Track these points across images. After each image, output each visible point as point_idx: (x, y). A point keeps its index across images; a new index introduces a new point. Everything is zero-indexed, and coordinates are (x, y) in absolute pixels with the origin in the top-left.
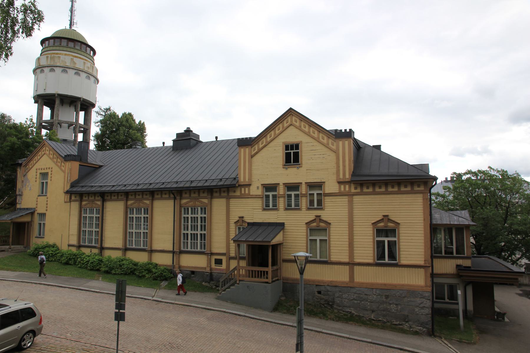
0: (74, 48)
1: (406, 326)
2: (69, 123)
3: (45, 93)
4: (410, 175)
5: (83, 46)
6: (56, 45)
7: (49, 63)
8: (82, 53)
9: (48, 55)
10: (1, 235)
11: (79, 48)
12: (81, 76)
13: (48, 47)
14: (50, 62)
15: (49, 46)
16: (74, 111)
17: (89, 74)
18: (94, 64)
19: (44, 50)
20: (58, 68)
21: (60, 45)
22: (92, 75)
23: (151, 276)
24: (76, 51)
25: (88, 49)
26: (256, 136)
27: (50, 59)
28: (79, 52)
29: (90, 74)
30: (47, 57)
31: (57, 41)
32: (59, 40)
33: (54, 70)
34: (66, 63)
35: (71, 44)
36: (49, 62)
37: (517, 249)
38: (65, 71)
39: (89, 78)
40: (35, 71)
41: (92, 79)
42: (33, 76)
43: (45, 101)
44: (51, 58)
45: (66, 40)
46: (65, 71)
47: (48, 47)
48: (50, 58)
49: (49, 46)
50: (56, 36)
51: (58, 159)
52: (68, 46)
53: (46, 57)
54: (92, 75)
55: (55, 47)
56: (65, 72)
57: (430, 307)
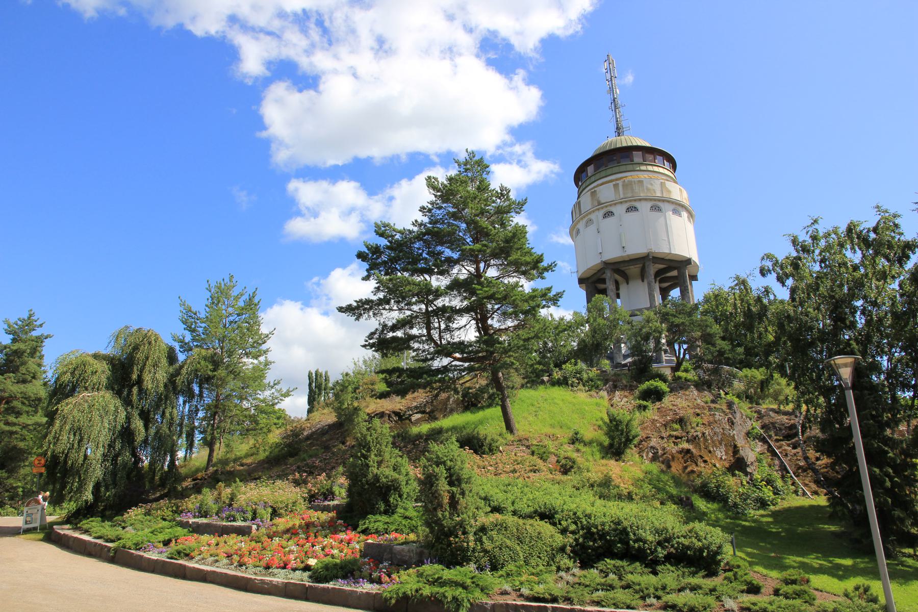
4: (663, 259)
7: (622, 196)
9: (618, 182)
10: (914, 422)
11: (641, 160)
12: (639, 209)
14: (624, 194)
17: (655, 200)
20: (644, 203)
22: (663, 201)
27: (623, 188)
29: (659, 200)
30: (616, 186)
33: (377, 233)
34: (655, 192)
36: (621, 192)
37: (484, 354)
39: (659, 209)
44: (625, 186)
45: (640, 153)
48: (623, 185)
53: (612, 186)
54: (663, 201)
57: (462, 469)
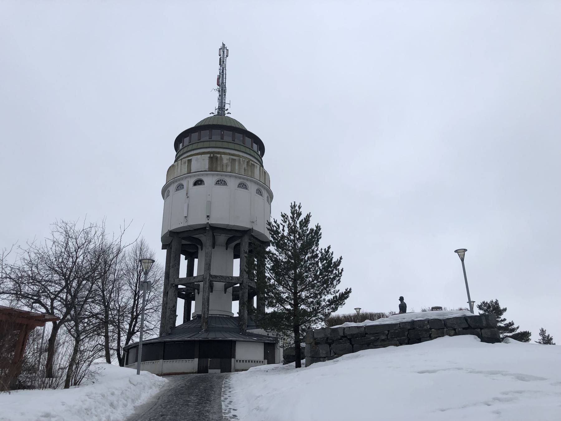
0: (211, 140)
1: (203, 306)
2: (227, 280)
3: (186, 225)
5: (239, 136)
6: (214, 138)
8: (237, 147)
11: (230, 139)
13: (188, 146)
15: (191, 143)
16: (232, 255)
18: (263, 167)
19: (178, 155)
21: (199, 140)
23: (37, 282)
24: (225, 145)
25: (248, 140)
26: (248, 130)
28: (232, 146)
31: (205, 134)
32: (207, 132)
35: (228, 136)
38: (243, 186)
40: (165, 192)
41: (265, 194)
42: (161, 201)
43: (184, 242)
46: (243, 186)
47: (188, 146)
49: (191, 143)
50: (215, 123)
51: (152, 323)
52: (223, 139)
55: (202, 143)
56: (244, 187)
